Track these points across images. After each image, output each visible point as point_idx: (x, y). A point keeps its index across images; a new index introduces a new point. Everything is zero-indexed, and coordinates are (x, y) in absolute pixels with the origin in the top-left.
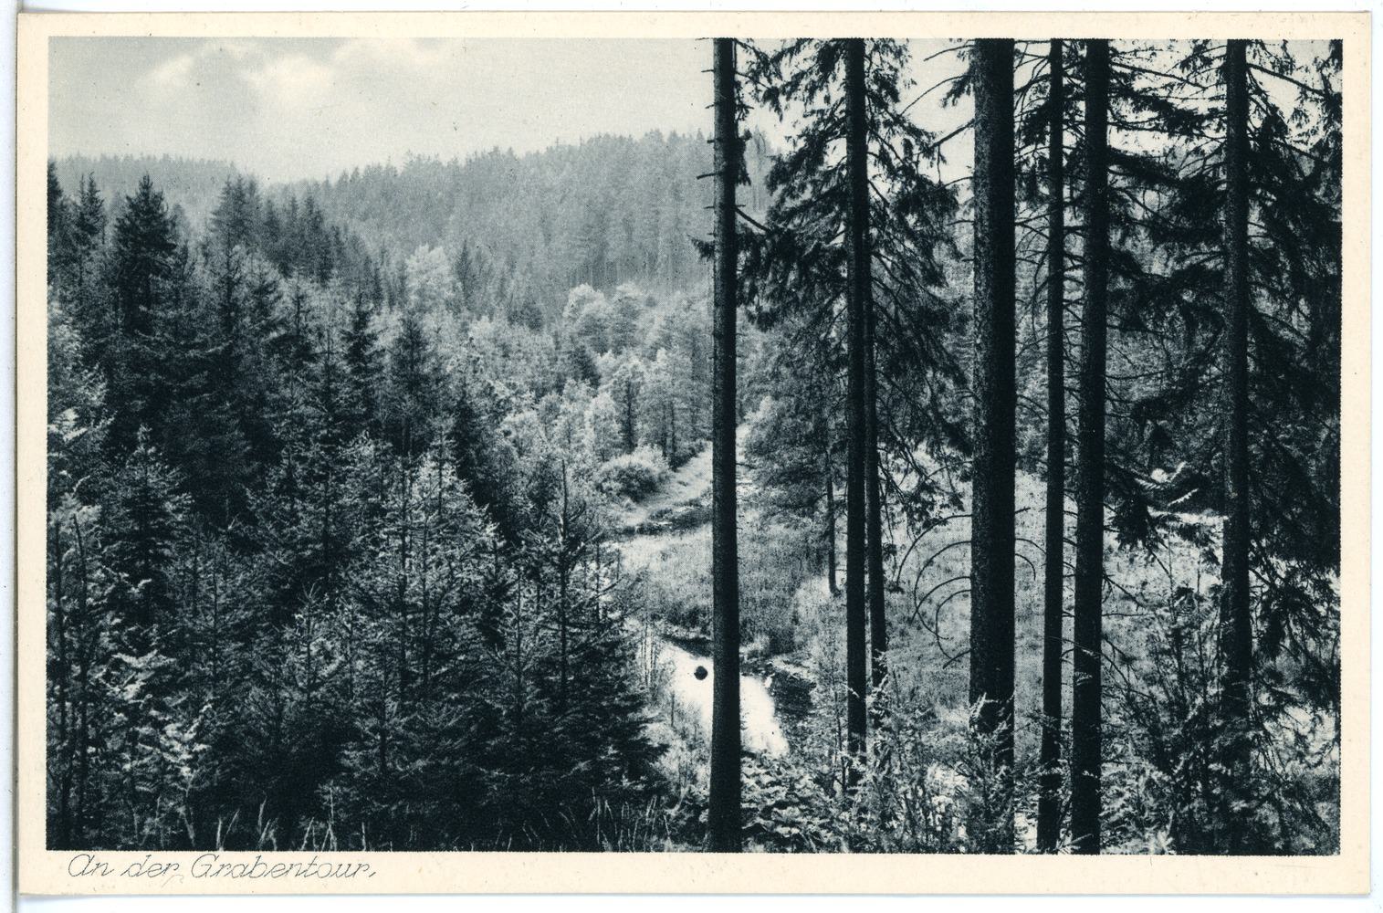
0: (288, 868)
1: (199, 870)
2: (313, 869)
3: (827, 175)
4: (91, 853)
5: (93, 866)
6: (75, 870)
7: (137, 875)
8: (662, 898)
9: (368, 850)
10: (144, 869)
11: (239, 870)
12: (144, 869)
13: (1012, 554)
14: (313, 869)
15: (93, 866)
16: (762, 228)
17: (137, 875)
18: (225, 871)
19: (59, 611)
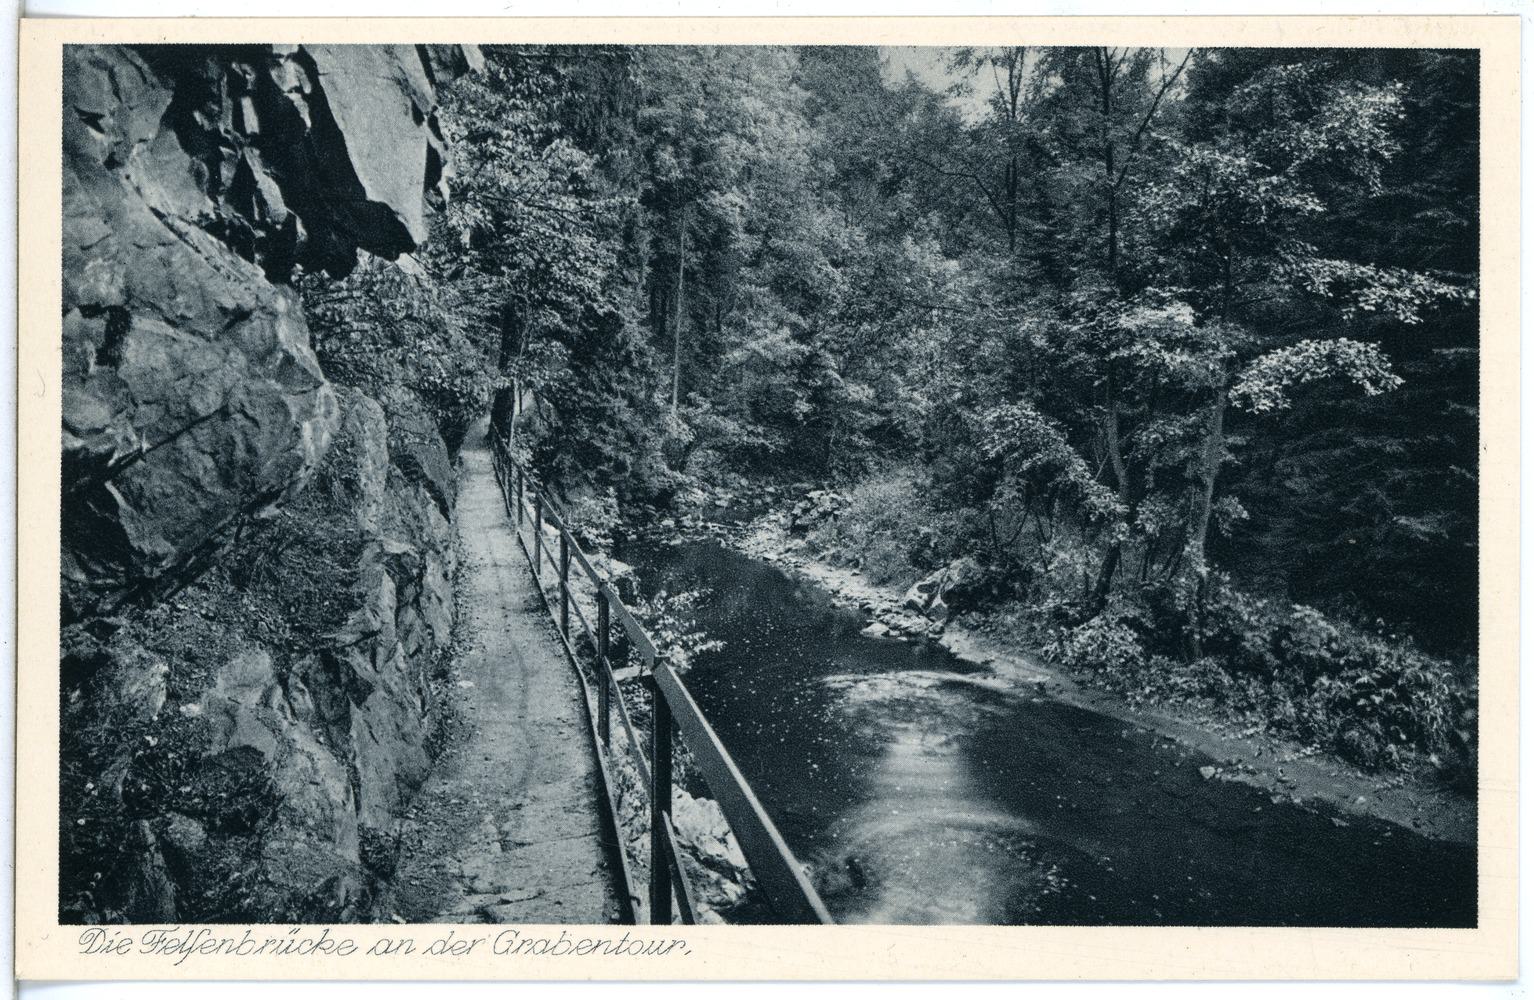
0: (219, 943)
1: (502, 945)
5: (517, 942)
7: (386, 952)
12: (447, 947)
17: (543, 952)
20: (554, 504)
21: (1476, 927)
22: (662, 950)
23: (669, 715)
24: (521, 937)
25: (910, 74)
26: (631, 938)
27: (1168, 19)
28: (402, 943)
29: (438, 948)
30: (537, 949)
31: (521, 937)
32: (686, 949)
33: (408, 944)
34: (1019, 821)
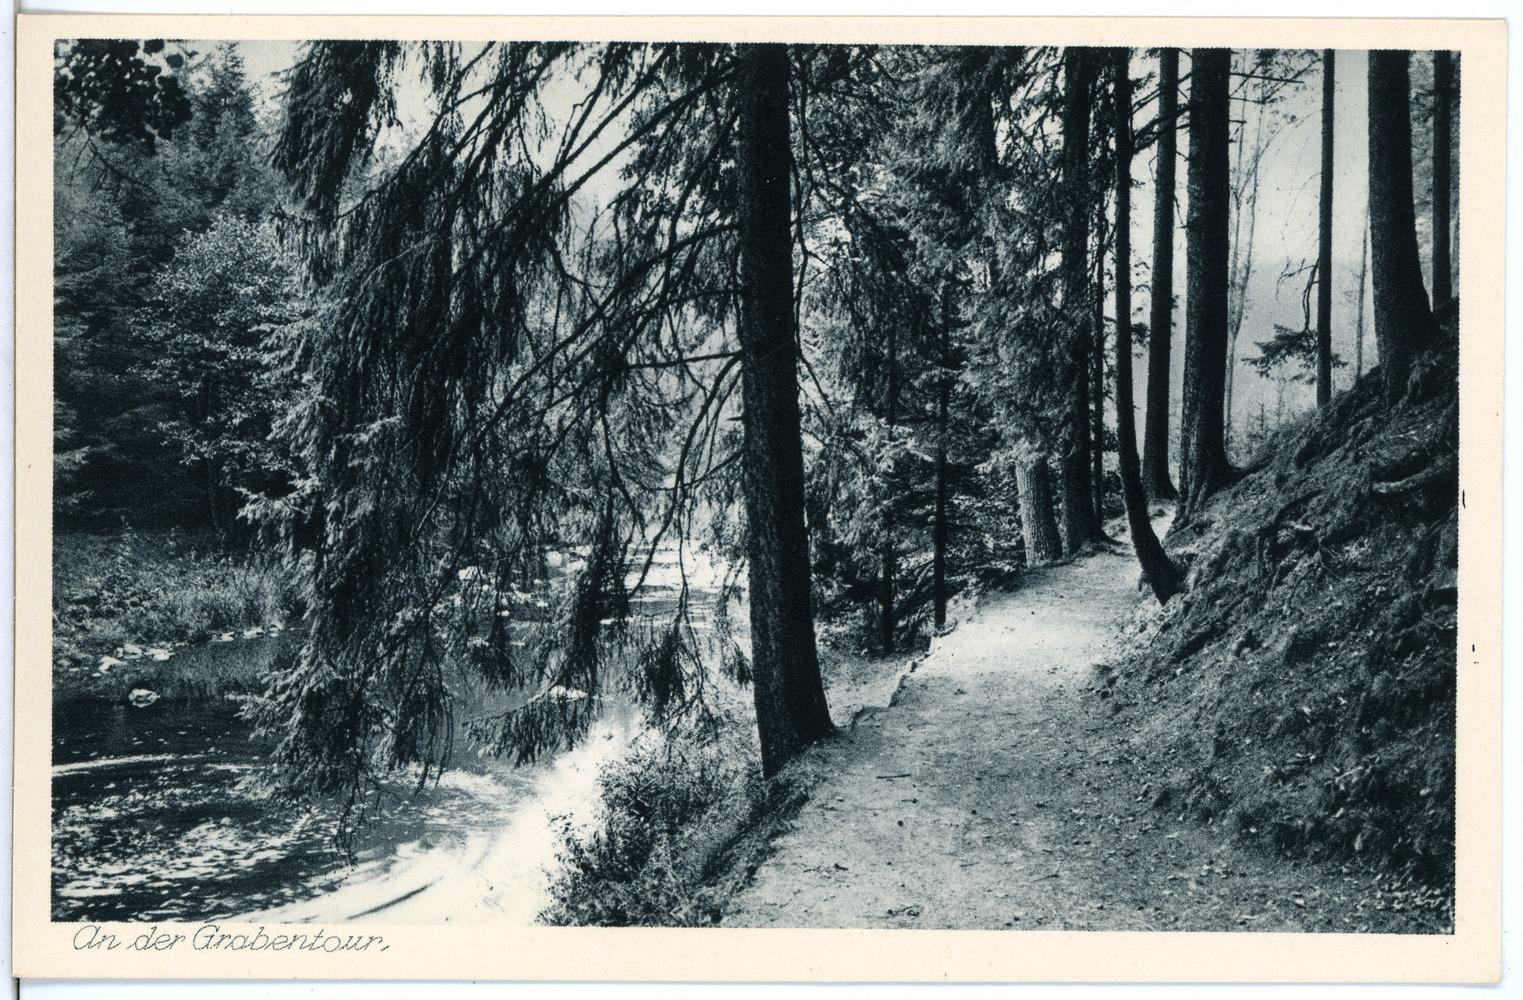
0: (291, 940)
1: (201, 941)
2: (320, 942)
3: (508, 513)
4: (97, 924)
5: (99, 938)
6: (82, 940)
7: (89, 945)
8: (1197, 988)
9: (58, 292)
10: (152, 942)
11: (239, 942)
12: (152, 942)
13: (1414, 233)
14: (320, 942)
15: (99, 938)
16: (577, 185)
17: (89, 945)
18: (226, 941)
19: (296, 896)
20: (269, 319)
21: (1436, 918)
22: (359, 945)
23: (153, 524)
24: (221, 932)
25: (1279, 328)
26: (325, 935)
27: (942, 979)
28: (295, 938)
29: (142, 943)
30: (236, 945)
31: (221, 932)
32: (383, 945)
33: (302, 940)
34: (1431, 265)
